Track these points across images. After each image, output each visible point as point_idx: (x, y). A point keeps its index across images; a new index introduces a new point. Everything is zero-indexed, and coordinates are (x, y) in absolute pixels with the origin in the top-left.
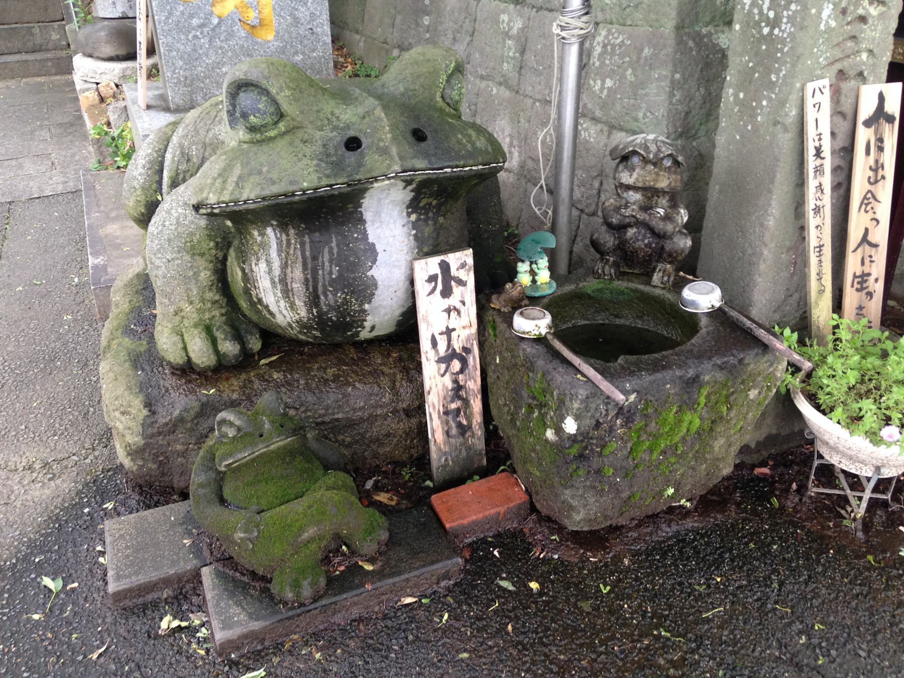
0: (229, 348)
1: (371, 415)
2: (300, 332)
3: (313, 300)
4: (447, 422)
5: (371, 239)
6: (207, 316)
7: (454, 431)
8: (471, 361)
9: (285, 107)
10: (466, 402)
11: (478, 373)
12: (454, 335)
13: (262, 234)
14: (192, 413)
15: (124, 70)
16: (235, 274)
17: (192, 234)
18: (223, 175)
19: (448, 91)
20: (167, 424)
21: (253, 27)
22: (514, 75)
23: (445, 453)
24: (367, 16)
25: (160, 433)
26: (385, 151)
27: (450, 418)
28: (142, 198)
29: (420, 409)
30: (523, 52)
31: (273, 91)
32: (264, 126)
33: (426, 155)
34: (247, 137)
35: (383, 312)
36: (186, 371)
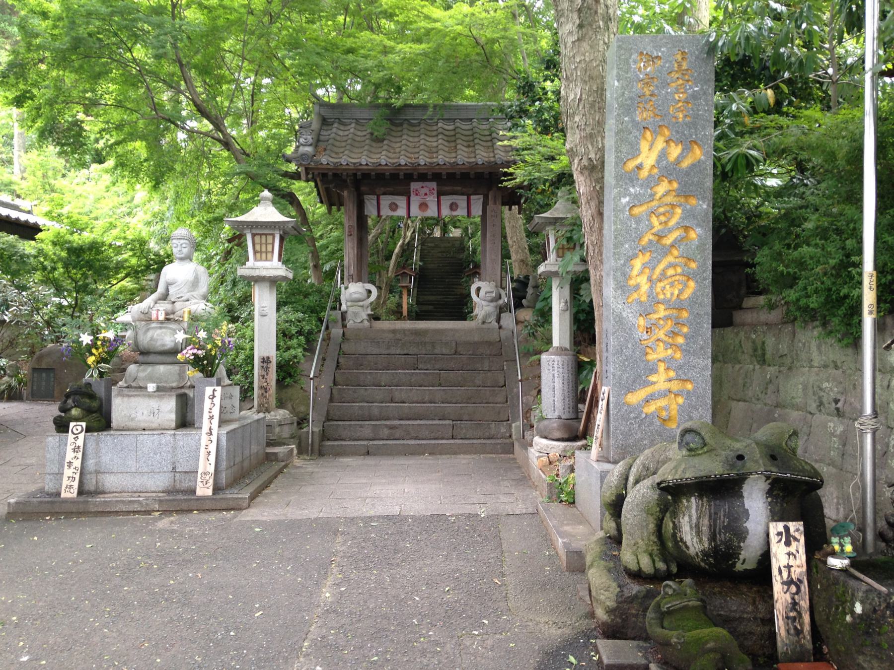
0: (661, 566)
1: (740, 618)
2: (703, 560)
3: (713, 538)
4: (788, 624)
5: (746, 507)
6: (650, 548)
7: (792, 631)
8: (802, 588)
9: (708, 440)
10: (800, 614)
11: (807, 597)
12: (792, 569)
13: (688, 501)
14: (642, 594)
15: (566, 447)
16: (668, 525)
17: (649, 502)
18: (676, 468)
19: (789, 443)
20: (629, 597)
21: (665, 420)
22: (838, 460)
23: (786, 645)
24: (730, 424)
25: (625, 602)
26: (757, 461)
27: (790, 621)
28: (615, 492)
29: (771, 621)
30: (844, 445)
31: (703, 433)
32: (697, 449)
33: (777, 466)
34: (688, 453)
35: (750, 550)
36: (637, 575)
